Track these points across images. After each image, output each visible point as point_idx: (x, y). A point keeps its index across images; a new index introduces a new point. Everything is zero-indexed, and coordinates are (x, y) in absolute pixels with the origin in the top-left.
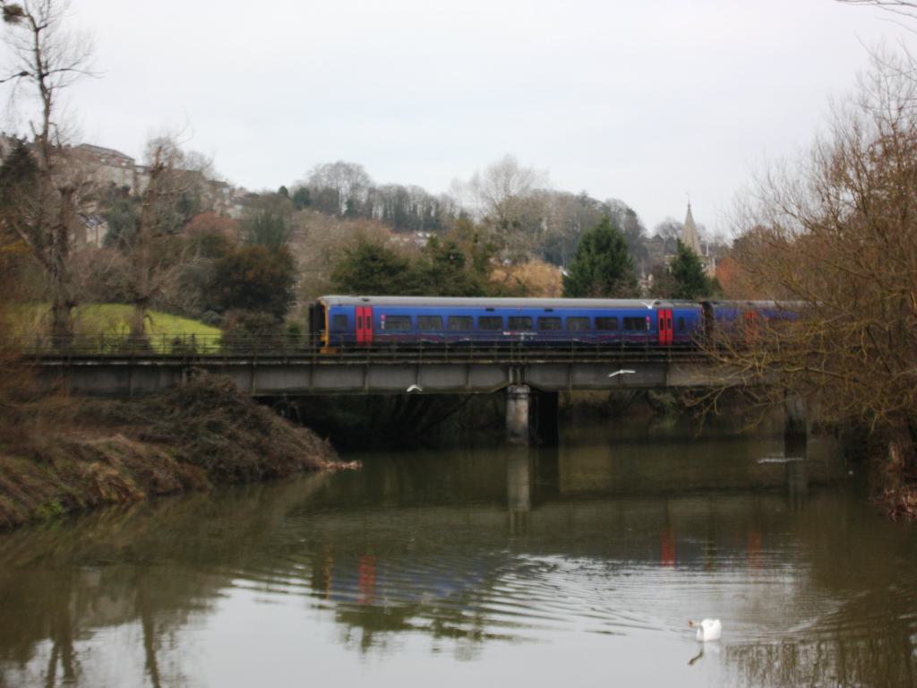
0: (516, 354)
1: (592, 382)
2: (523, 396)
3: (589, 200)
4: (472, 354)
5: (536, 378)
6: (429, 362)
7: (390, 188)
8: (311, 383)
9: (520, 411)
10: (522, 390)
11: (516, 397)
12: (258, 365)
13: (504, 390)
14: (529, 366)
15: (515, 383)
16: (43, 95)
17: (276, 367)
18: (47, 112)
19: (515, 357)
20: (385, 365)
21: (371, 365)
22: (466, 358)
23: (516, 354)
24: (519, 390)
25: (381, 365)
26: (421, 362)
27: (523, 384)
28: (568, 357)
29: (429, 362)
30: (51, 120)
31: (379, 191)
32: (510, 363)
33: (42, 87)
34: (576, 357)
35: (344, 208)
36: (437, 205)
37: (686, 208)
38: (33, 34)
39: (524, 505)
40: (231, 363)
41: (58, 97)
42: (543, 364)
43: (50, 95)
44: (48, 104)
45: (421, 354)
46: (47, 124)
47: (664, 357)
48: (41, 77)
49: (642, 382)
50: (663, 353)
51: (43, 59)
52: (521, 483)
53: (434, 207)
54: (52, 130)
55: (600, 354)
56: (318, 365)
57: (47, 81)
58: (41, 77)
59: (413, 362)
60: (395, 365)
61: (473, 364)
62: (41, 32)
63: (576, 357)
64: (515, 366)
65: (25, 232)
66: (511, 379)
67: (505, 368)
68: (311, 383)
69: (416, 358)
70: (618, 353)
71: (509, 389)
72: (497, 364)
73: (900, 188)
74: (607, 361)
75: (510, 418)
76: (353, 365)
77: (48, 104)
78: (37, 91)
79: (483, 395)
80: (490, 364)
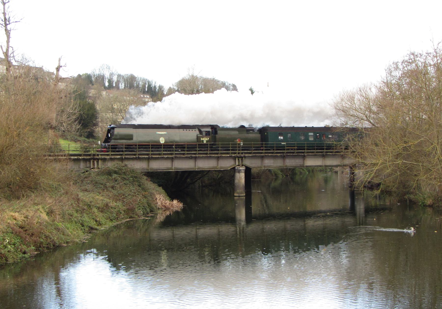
0: (239, 152)
1: (272, 165)
2: (243, 171)
3: (216, 80)
4: (220, 152)
5: (248, 162)
6: (201, 156)
7: (352, 99)
8: (148, 166)
9: (241, 178)
10: (243, 168)
11: (239, 171)
12: (125, 158)
13: (234, 168)
14: (245, 157)
15: (238, 165)
16: (6, 34)
17: (133, 159)
18: (8, 42)
19: (239, 153)
20: (182, 157)
21: (175, 157)
22: (217, 154)
23: (239, 152)
24: (241, 168)
25: (180, 157)
26: (197, 156)
27: (243, 165)
28: (261, 153)
29: (201, 156)
30: (10, 44)
31: (122, 76)
32: (237, 156)
33: (6, 30)
34: (265, 153)
35: (107, 84)
36: (149, 82)
37: (229, 81)
38: (2, 6)
39: (243, 223)
40: (113, 157)
41: (12, 34)
42: (251, 156)
43: (9, 33)
44: (8, 37)
45: (198, 152)
46: (8, 47)
47: (303, 153)
48: (6, 25)
49: (294, 164)
50: (303, 151)
51: (7, 17)
52: (241, 215)
53: (147, 83)
54: (10, 50)
55: (276, 151)
56: (152, 157)
57: (9, 27)
58: (6, 25)
59: (194, 156)
60: (186, 157)
61: (221, 156)
62: (6, 4)
63: (265, 153)
64: (239, 157)
65: (432, 115)
66: (237, 164)
67: (234, 158)
68: (148, 166)
69: (195, 154)
70: (284, 151)
71: (236, 168)
72: (231, 156)
73: (410, 89)
74: (278, 155)
75: (236, 181)
76: (168, 157)
77: (8, 37)
78: (4, 32)
79: (224, 172)
80: (228, 156)
